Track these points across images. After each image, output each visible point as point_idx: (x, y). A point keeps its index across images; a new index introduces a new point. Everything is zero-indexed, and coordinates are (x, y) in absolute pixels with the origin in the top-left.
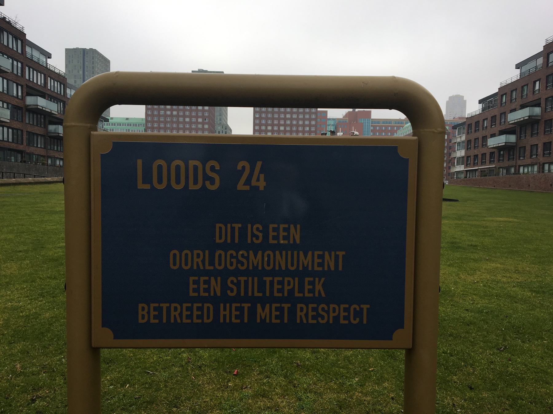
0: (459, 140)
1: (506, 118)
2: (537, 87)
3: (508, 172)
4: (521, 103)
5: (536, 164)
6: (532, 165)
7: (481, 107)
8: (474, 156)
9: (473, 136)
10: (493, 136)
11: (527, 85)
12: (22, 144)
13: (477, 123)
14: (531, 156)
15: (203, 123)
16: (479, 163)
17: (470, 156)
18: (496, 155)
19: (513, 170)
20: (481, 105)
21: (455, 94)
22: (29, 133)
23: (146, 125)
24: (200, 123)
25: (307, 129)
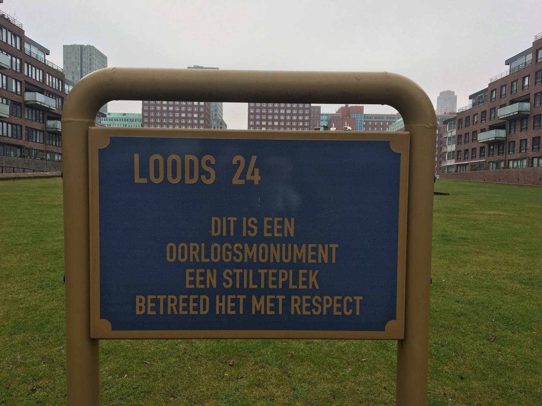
0: (449, 135)
15: (199, 119)
16: (478, 156)
22: (28, 128)
23: (143, 120)
24: (196, 118)
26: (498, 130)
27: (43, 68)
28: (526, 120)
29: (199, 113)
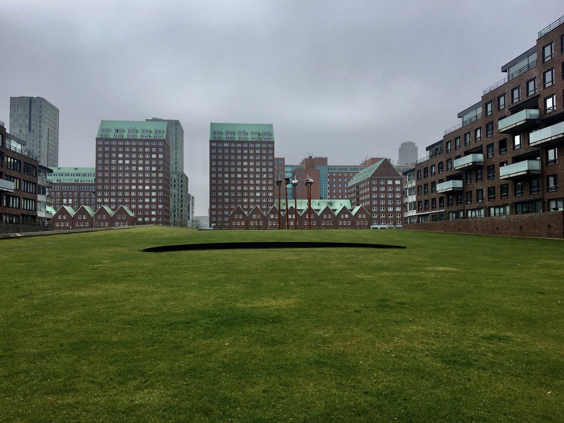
1: (452, 165)
2: (478, 135)
3: (457, 217)
4: (465, 150)
5: (482, 208)
6: (479, 209)
7: (428, 154)
8: (425, 201)
9: (423, 182)
10: (441, 181)
11: (469, 133)
13: (426, 169)
14: (478, 200)
15: (157, 172)
16: (423, 209)
17: (421, 201)
18: (445, 200)
19: (461, 214)
20: (428, 152)
21: (407, 141)
24: (154, 172)
25: (265, 176)
29: (157, 166)
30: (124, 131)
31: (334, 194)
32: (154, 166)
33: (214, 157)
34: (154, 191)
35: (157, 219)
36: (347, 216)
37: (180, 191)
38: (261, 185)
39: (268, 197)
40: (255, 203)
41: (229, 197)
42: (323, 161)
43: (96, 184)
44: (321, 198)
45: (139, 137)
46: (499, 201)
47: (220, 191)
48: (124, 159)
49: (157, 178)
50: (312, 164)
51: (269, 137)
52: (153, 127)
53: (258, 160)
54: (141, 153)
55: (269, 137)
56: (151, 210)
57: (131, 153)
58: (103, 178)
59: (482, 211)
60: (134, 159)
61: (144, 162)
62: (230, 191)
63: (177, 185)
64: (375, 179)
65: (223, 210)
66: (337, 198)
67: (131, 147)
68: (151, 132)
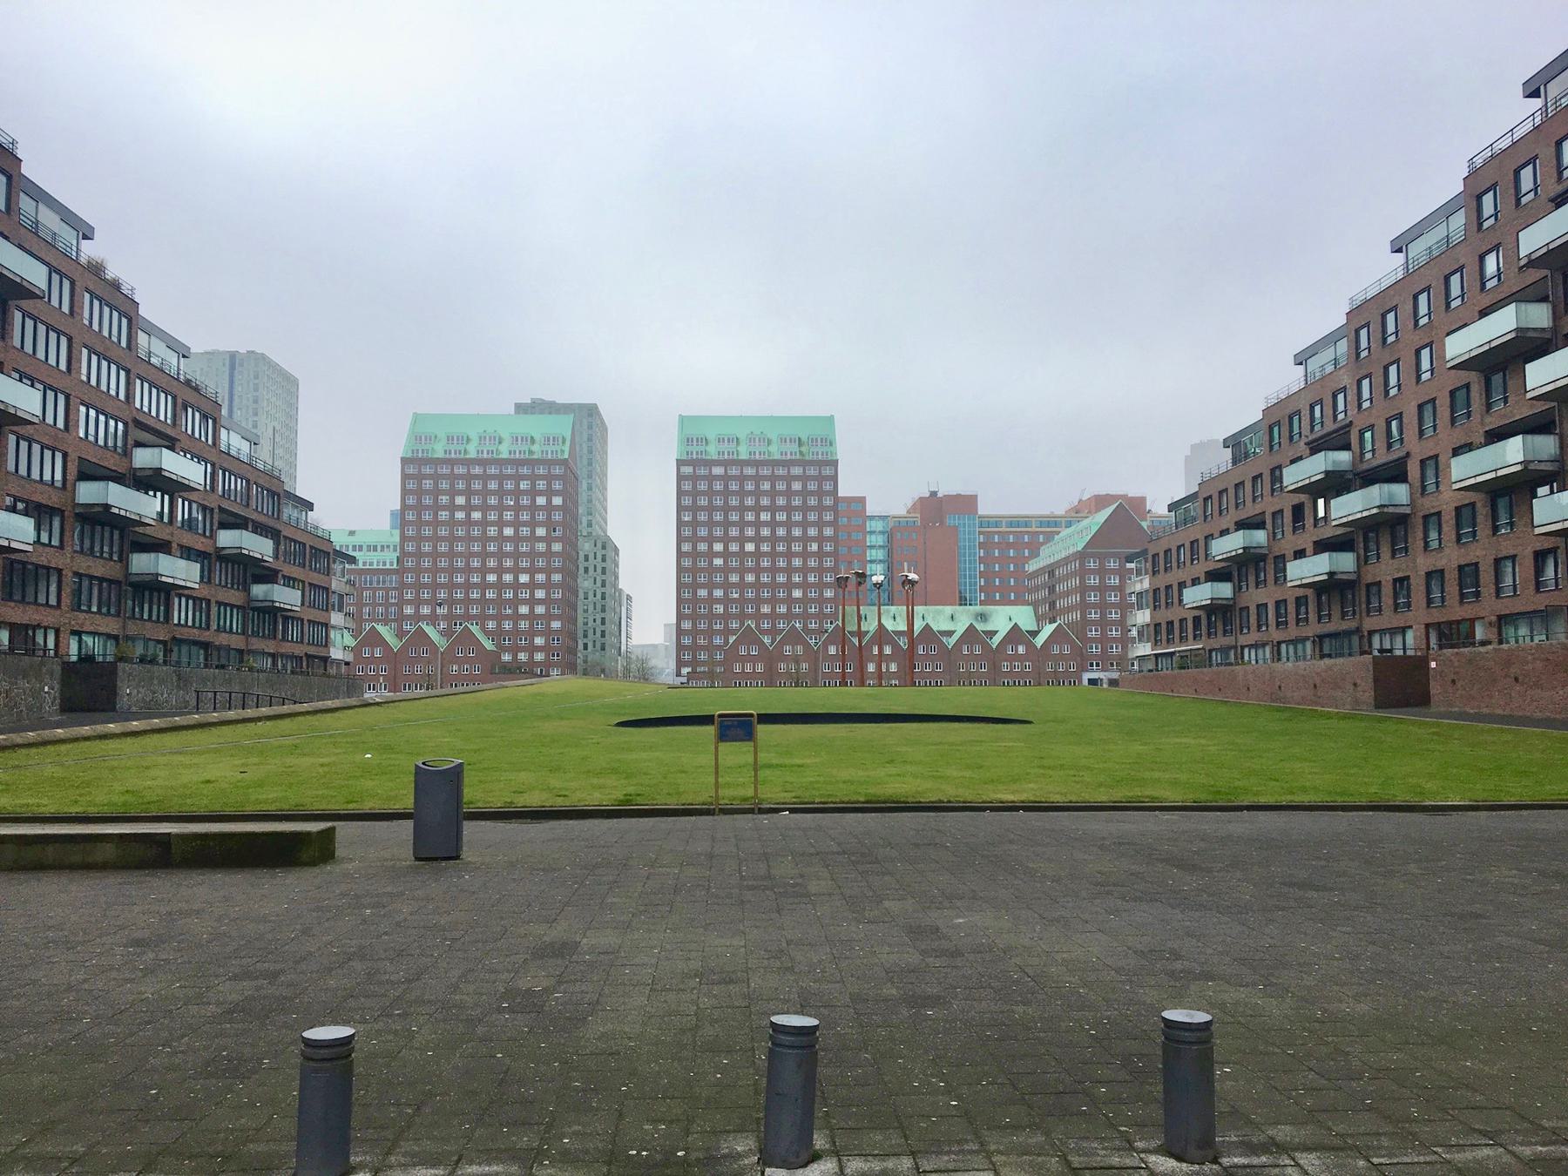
0: (1138, 588)
9: (1163, 580)
12: (208, 627)
15: (548, 540)
16: (1177, 640)
22: (219, 604)
23: (402, 548)
24: (540, 539)
26: (1334, 554)
27: (248, 476)
28: (1252, 571)
29: (551, 527)
30: (468, 440)
31: (998, 589)
32: (541, 524)
33: (687, 486)
34: (540, 586)
35: (547, 656)
36: (1021, 650)
37: (599, 583)
38: (804, 570)
39: (821, 601)
40: (789, 616)
41: (726, 601)
42: (966, 503)
43: (401, 571)
44: (963, 601)
45: (505, 455)
46: (1293, 631)
47: (703, 586)
48: (468, 508)
49: (549, 554)
50: (938, 510)
51: (825, 449)
52: (539, 427)
53: (796, 508)
54: (509, 492)
55: (825, 449)
56: (532, 633)
57: (485, 493)
58: (419, 555)
59: (1268, 649)
60: (493, 508)
61: (517, 516)
62: (726, 586)
63: (591, 569)
64: (1093, 555)
65: (710, 633)
66: (1005, 602)
67: (485, 478)
68: (533, 441)
